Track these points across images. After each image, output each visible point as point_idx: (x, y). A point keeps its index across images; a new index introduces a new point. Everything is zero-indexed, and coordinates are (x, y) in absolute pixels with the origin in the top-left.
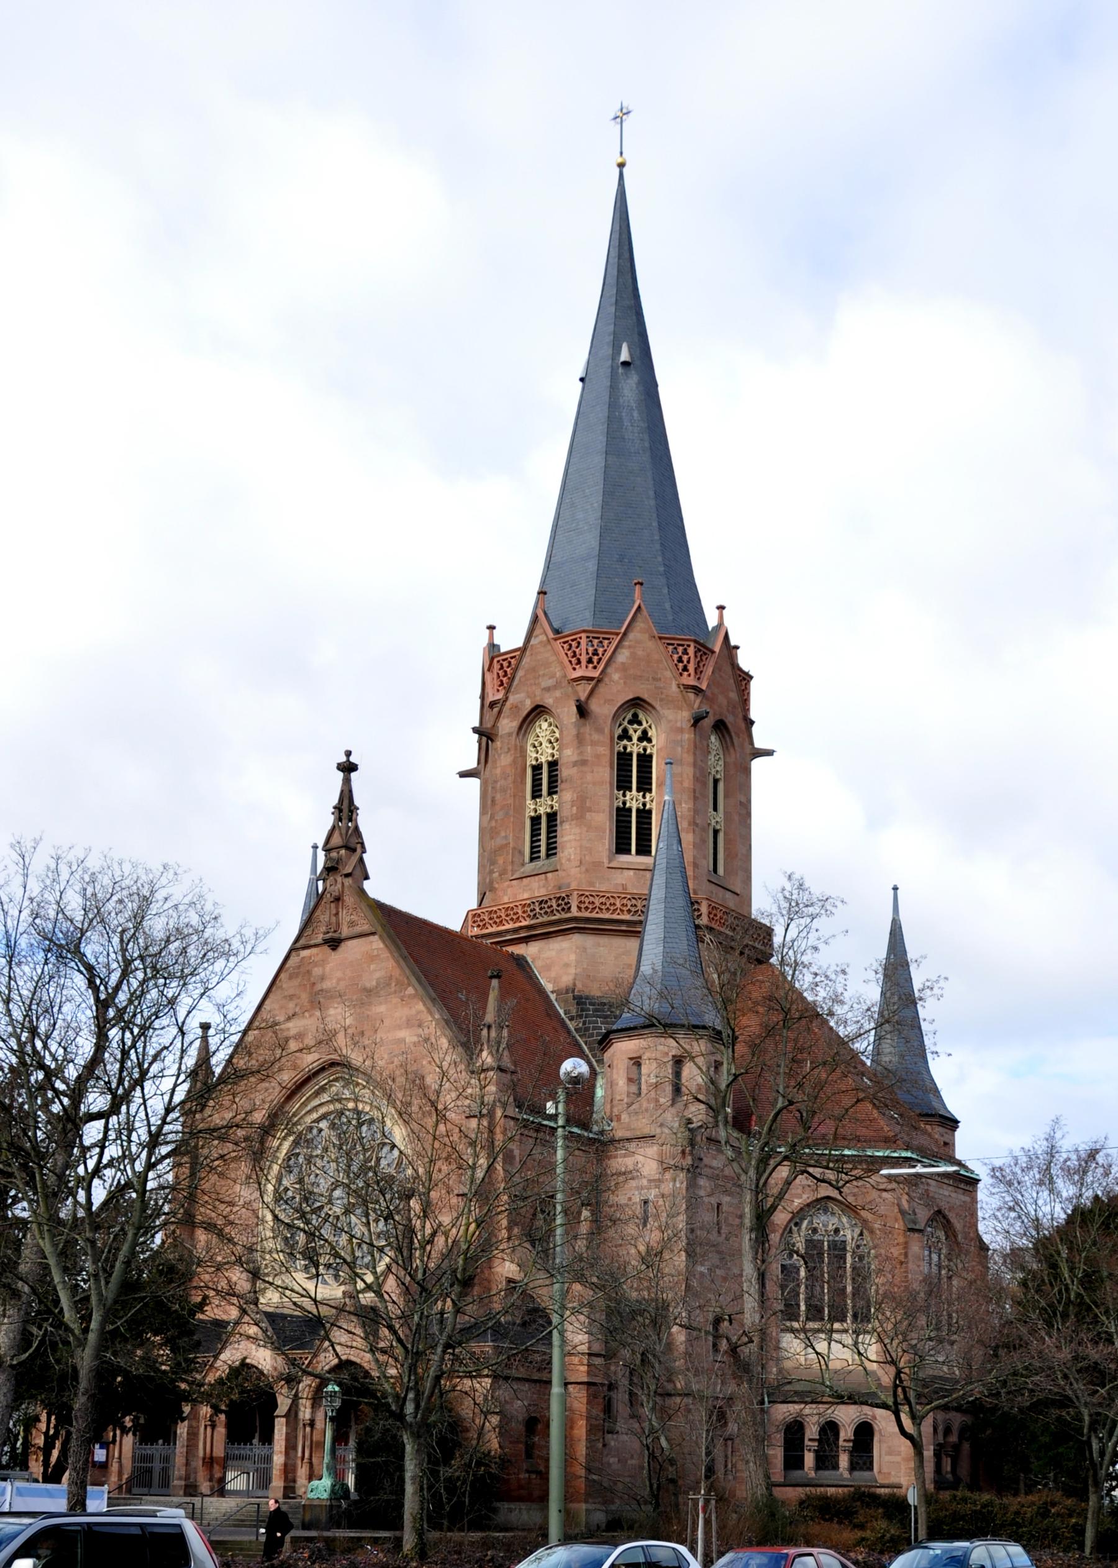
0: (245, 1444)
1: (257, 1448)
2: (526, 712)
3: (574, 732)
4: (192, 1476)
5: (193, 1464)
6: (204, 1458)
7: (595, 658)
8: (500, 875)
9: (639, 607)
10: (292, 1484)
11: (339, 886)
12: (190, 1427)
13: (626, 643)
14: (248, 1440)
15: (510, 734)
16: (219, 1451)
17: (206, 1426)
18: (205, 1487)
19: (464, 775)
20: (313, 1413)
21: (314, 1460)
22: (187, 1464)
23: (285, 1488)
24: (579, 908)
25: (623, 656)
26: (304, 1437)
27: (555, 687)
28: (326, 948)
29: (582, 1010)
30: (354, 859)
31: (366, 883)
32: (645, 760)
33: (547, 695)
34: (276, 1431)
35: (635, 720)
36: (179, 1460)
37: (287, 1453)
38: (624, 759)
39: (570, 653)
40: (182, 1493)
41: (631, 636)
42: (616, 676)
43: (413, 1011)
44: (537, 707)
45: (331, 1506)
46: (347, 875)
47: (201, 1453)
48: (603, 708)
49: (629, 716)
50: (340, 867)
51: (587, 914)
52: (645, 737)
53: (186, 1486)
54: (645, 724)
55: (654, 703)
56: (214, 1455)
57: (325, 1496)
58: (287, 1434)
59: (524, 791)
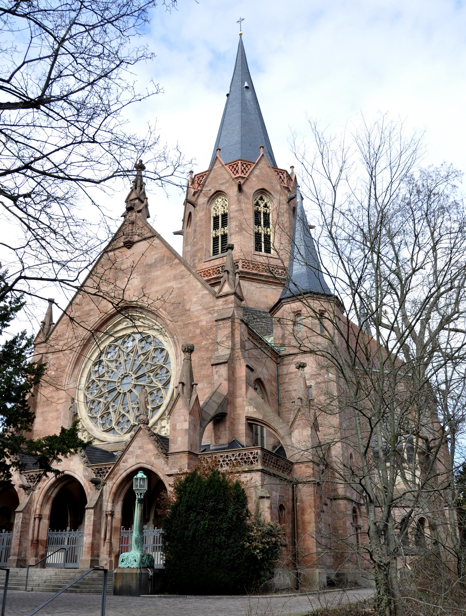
0: (62, 531)
1: (67, 534)
2: (211, 194)
3: (236, 198)
4: (23, 553)
5: (24, 545)
6: (32, 541)
7: (245, 172)
8: (199, 261)
9: (263, 155)
10: (96, 558)
11: (134, 217)
12: (24, 518)
13: (258, 167)
14: (63, 528)
15: (204, 204)
16: (43, 536)
17: (35, 518)
18: (32, 561)
19: (176, 233)
20: (113, 506)
21: (113, 540)
22: (20, 544)
23: (92, 561)
24: (243, 267)
25: (257, 172)
26: (106, 524)
27: (226, 183)
28: (125, 249)
29: (246, 312)
30: (143, 205)
31: (149, 220)
32: (266, 215)
33: (222, 186)
34: (86, 519)
35: (261, 199)
36: (15, 542)
37: (94, 535)
38: (257, 214)
39: (233, 170)
40: (15, 565)
41: (260, 165)
42: (254, 179)
43: (178, 271)
44: (217, 191)
45: (141, 574)
46: (139, 211)
47: (30, 537)
48: (250, 189)
49: (259, 197)
50: (135, 208)
51: (246, 270)
52: (266, 206)
53: (18, 560)
54: (266, 201)
55: (271, 192)
56: (40, 538)
57: (135, 565)
58: (94, 521)
59: (210, 226)
